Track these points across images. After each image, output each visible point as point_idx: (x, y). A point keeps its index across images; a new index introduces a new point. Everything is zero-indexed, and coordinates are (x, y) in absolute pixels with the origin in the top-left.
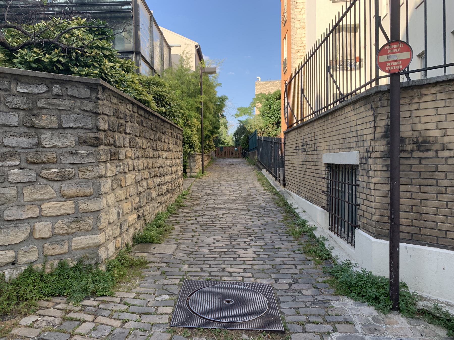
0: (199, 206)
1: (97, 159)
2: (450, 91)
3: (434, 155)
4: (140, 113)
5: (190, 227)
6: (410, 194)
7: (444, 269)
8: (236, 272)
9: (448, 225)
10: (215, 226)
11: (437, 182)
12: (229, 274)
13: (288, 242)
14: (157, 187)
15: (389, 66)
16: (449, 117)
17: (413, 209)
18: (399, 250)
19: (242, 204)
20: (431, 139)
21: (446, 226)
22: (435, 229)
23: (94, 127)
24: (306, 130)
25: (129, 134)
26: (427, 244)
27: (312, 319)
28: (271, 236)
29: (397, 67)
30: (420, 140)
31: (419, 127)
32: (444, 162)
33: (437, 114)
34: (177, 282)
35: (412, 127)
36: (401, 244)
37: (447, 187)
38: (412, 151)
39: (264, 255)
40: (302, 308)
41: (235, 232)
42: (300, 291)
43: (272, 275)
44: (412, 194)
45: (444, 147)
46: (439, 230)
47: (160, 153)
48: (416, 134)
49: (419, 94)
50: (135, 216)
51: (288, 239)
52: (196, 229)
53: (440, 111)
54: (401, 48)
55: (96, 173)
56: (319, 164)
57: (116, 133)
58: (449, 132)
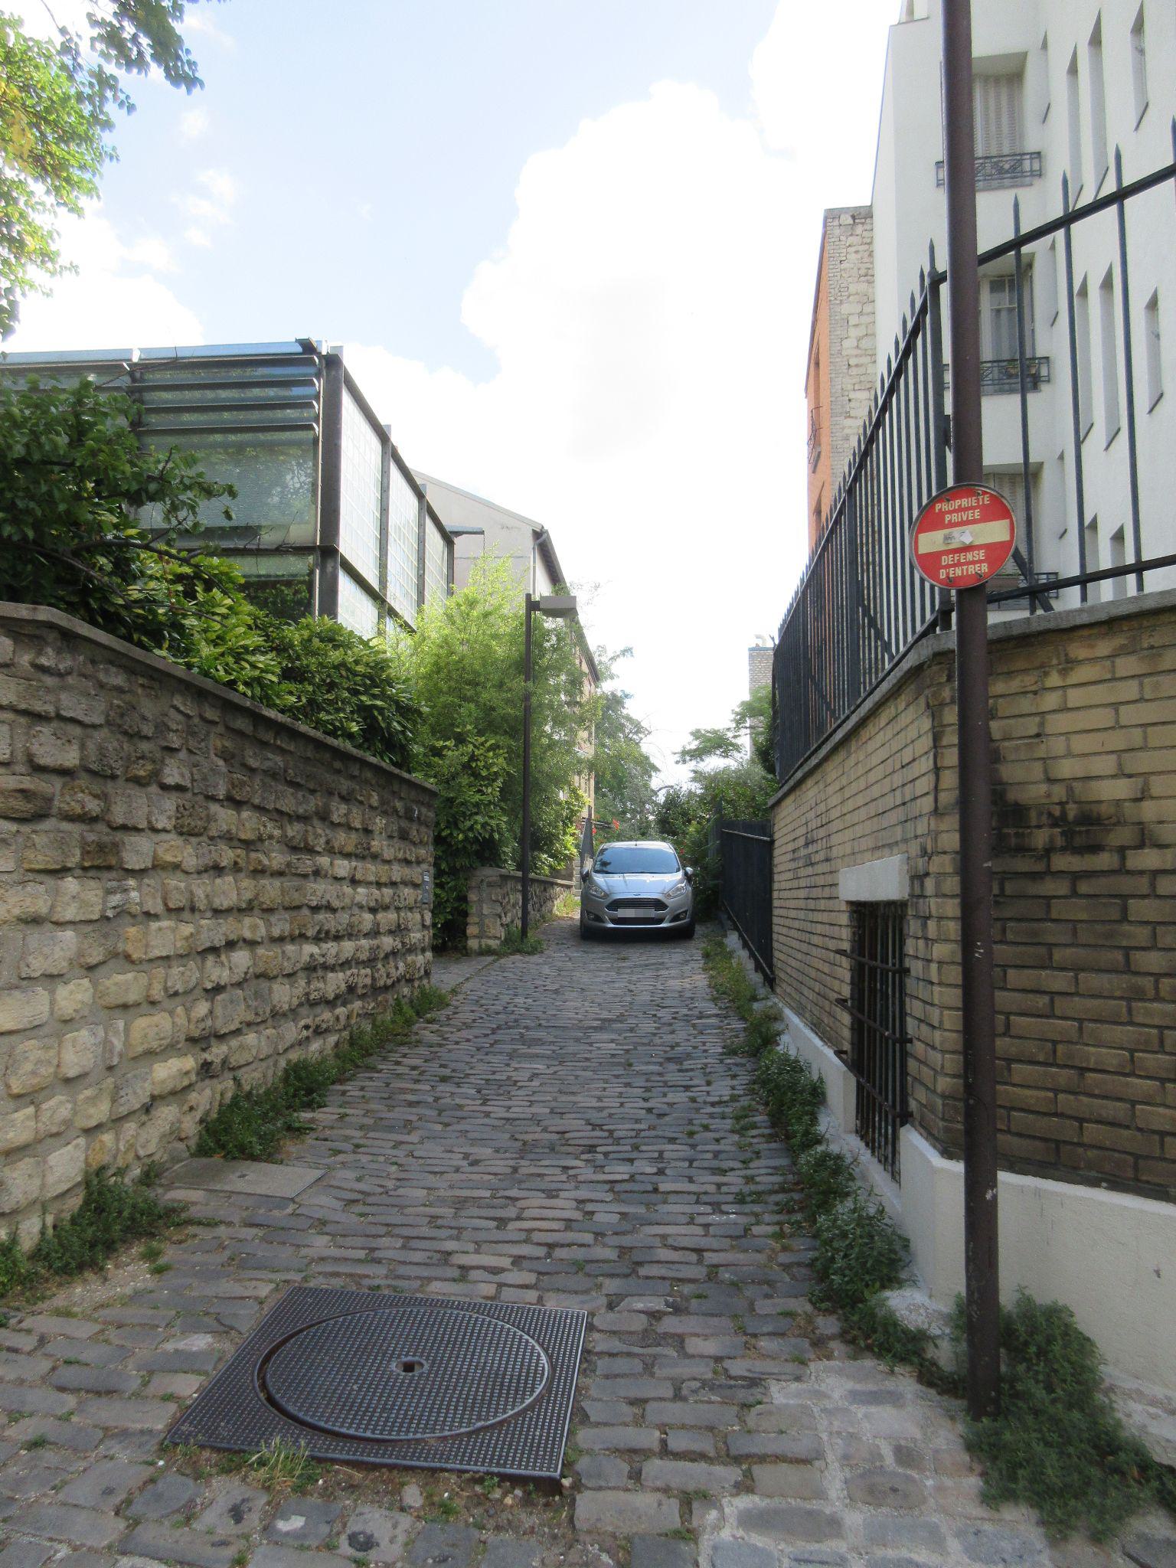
0: (464, 1046)
1: (21, 860)
2: (1152, 647)
3: (1116, 866)
4: (232, 725)
5: (400, 1114)
6: (1046, 999)
7: (1158, 1273)
8: (484, 1268)
9: (1167, 1111)
10: (487, 1115)
11: (1127, 957)
12: (456, 1273)
13: (714, 1174)
14: (301, 974)
15: (948, 566)
16: (1156, 736)
17: (1059, 1053)
18: (995, 1197)
19: (613, 1045)
20: (1105, 810)
21: (1159, 1117)
22: (1128, 1127)
23: (20, 756)
24: (811, 793)
25: (179, 788)
26: (1105, 1181)
27: (677, 1442)
28: (661, 1153)
29: (972, 569)
30: (1072, 811)
31: (1067, 769)
32: (1145, 890)
33: (1118, 726)
34: (264, 1290)
35: (1046, 771)
36: (1004, 1177)
37: (1157, 976)
38: (1049, 851)
39: (606, 1216)
40: (661, 1399)
41: (547, 1136)
42: (679, 1341)
43: (607, 1282)
44: (1052, 1001)
45: (1145, 838)
46: (1140, 1130)
47: (324, 861)
48: (1059, 792)
49: (1063, 658)
50: (189, 1063)
51: (715, 1163)
52: (420, 1119)
53: (1128, 715)
54: (984, 509)
55: (15, 906)
56: (831, 904)
57: (121, 782)
58: (1157, 786)
